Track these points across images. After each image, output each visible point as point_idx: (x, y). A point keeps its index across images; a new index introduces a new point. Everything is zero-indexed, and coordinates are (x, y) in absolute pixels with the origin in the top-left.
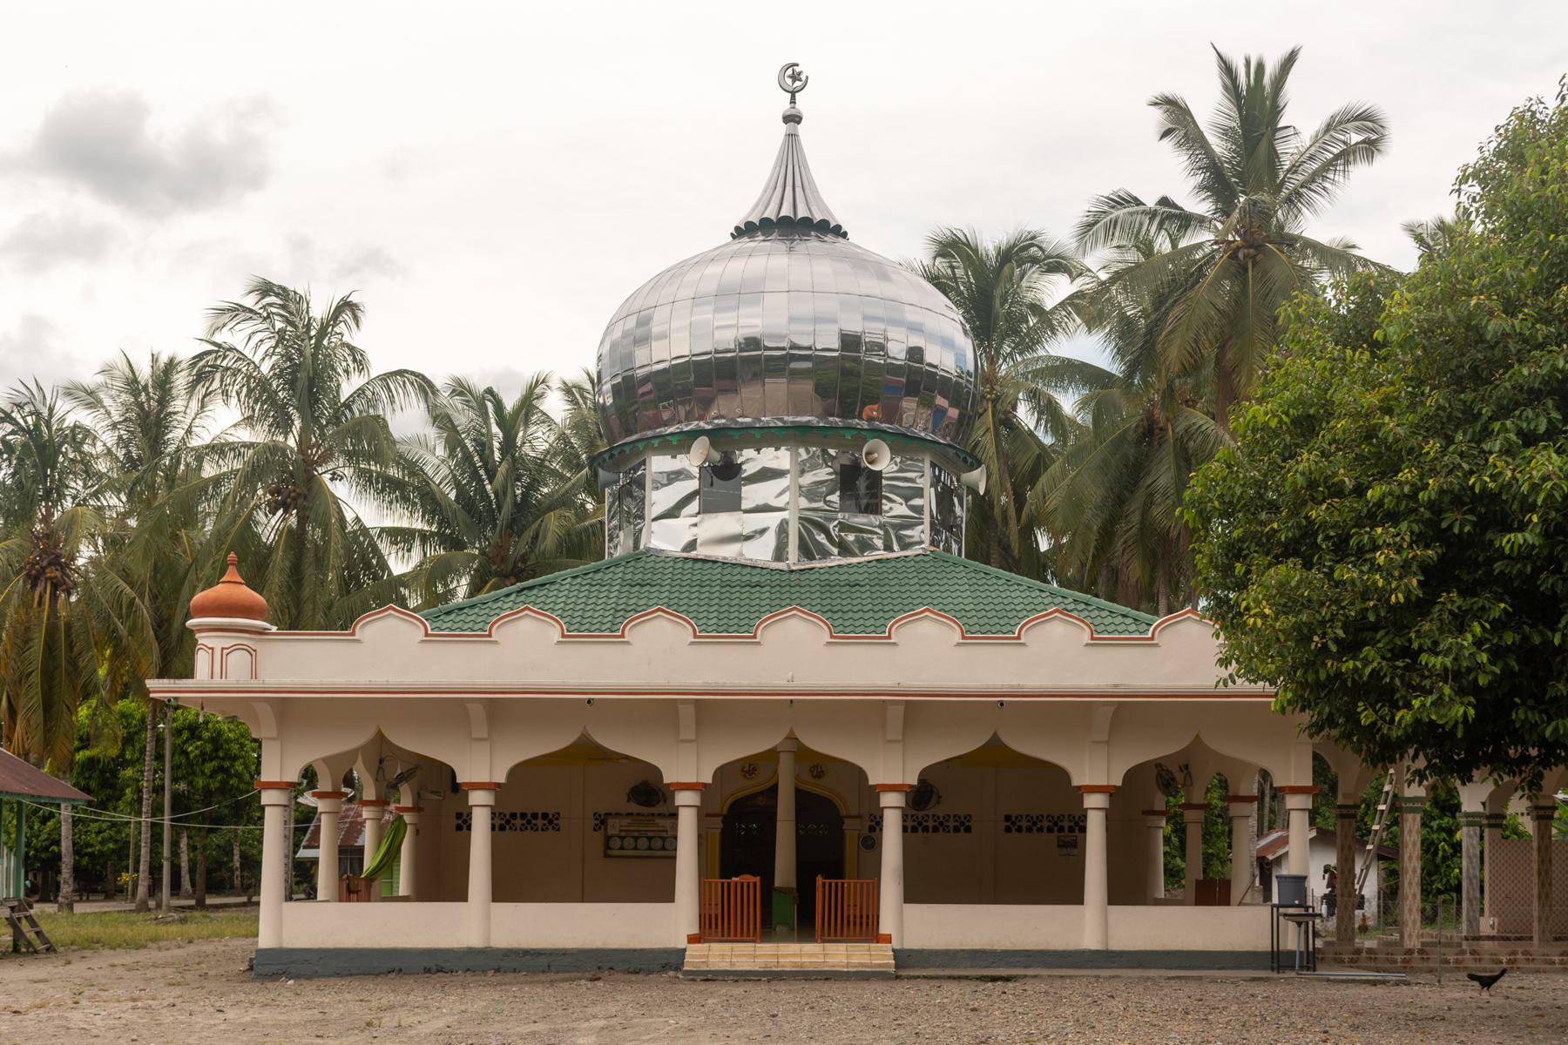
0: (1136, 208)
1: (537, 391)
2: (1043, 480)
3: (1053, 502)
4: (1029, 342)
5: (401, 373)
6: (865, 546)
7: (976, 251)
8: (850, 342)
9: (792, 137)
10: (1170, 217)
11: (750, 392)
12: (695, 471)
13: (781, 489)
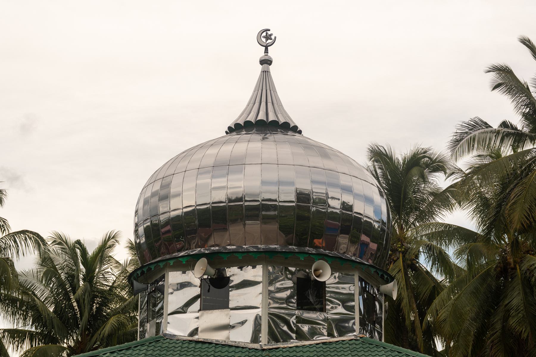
0: (486, 130)
1: (110, 243)
2: (436, 301)
3: (443, 314)
4: (424, 215)
5: (24, 232)
6: (313, 333)
7: (391, 158)
8: (303, 197)
9: (265, 74)
10: (508, 135)
11: (235, 229)
12: (198, 282)
13: (254, 297)
